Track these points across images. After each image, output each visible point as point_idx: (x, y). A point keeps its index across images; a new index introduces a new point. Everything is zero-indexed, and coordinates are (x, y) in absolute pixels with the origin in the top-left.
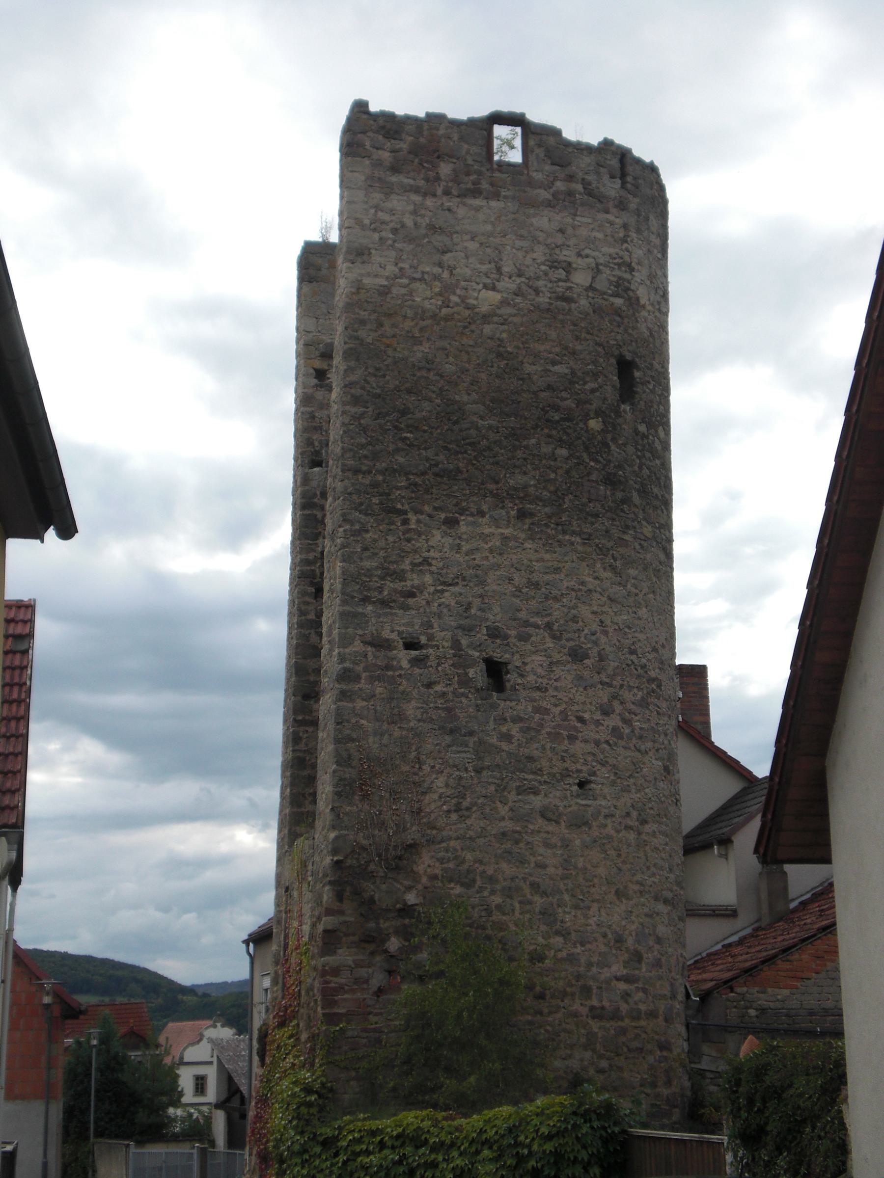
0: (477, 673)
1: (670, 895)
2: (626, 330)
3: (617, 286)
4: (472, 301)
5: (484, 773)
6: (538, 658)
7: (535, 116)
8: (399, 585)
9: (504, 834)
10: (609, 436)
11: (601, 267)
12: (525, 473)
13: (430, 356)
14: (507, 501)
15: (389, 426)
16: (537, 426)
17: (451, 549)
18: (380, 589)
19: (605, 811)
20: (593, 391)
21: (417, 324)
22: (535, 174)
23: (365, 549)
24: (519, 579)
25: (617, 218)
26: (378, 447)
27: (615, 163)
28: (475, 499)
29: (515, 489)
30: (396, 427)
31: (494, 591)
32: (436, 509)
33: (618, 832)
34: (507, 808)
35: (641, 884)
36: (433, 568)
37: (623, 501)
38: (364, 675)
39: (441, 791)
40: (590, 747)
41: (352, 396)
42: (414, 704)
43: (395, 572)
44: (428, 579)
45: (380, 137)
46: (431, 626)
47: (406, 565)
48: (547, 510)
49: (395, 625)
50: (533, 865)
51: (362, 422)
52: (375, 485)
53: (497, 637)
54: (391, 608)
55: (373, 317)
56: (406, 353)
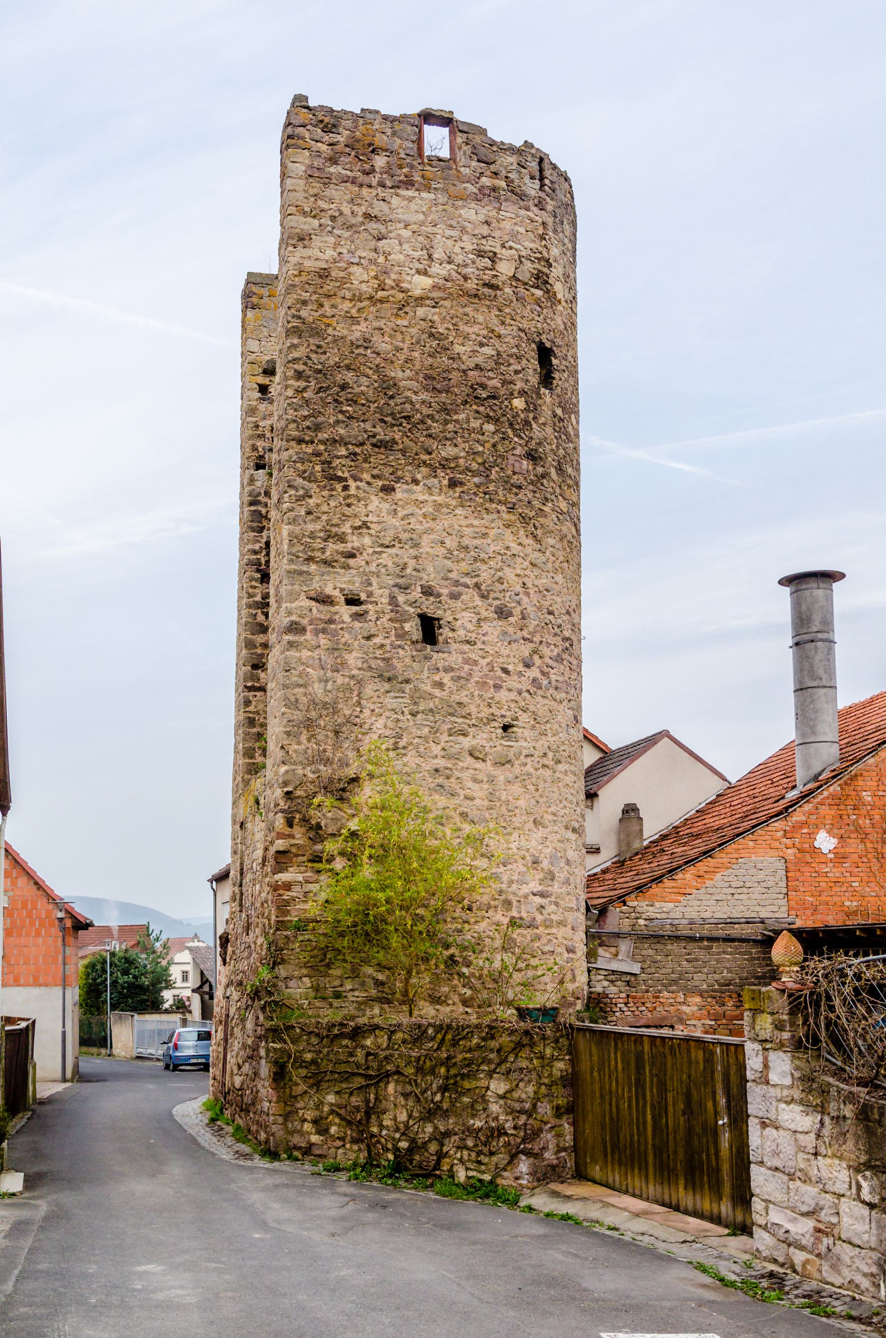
0: (413, 627)
1: (577, 825)
3: (538, 278)
5: (420, 716)
8: (340, 547)
9: (437, 770)
10: (531, 415)
12: (456, 446)
13: (367, 335)
14: (439, 471)
15: (330, 399)
16: (466, 402)
17: (389, 513)
19: (525, 752)
20: (517, 372)
21: (354, 306)
22: (462, 169)
23: (309, 513)
24: (450, 543)
26: (321, 419)
27: (534, 165)
28: (410, 468)
29: (447, 460)
30: (336, 401)
31: (427, 553)
32: (374, 477)
33: (536, 769)
34: (439, 747)
35: (555, 814)
36: (372, 532)
38: (309, 628)
39: (380, 732)
40: (513, 695)
41: (296, 371)
42: (354, 654)
43: (336, 535)
46: (370, 584)
48: (476, 480)
49: (334, 584)
50: (462, 797)
51: (305, 395)
53: (431, 595)
54: (333, 567)
55: (314, 297)
56: (345, 332)
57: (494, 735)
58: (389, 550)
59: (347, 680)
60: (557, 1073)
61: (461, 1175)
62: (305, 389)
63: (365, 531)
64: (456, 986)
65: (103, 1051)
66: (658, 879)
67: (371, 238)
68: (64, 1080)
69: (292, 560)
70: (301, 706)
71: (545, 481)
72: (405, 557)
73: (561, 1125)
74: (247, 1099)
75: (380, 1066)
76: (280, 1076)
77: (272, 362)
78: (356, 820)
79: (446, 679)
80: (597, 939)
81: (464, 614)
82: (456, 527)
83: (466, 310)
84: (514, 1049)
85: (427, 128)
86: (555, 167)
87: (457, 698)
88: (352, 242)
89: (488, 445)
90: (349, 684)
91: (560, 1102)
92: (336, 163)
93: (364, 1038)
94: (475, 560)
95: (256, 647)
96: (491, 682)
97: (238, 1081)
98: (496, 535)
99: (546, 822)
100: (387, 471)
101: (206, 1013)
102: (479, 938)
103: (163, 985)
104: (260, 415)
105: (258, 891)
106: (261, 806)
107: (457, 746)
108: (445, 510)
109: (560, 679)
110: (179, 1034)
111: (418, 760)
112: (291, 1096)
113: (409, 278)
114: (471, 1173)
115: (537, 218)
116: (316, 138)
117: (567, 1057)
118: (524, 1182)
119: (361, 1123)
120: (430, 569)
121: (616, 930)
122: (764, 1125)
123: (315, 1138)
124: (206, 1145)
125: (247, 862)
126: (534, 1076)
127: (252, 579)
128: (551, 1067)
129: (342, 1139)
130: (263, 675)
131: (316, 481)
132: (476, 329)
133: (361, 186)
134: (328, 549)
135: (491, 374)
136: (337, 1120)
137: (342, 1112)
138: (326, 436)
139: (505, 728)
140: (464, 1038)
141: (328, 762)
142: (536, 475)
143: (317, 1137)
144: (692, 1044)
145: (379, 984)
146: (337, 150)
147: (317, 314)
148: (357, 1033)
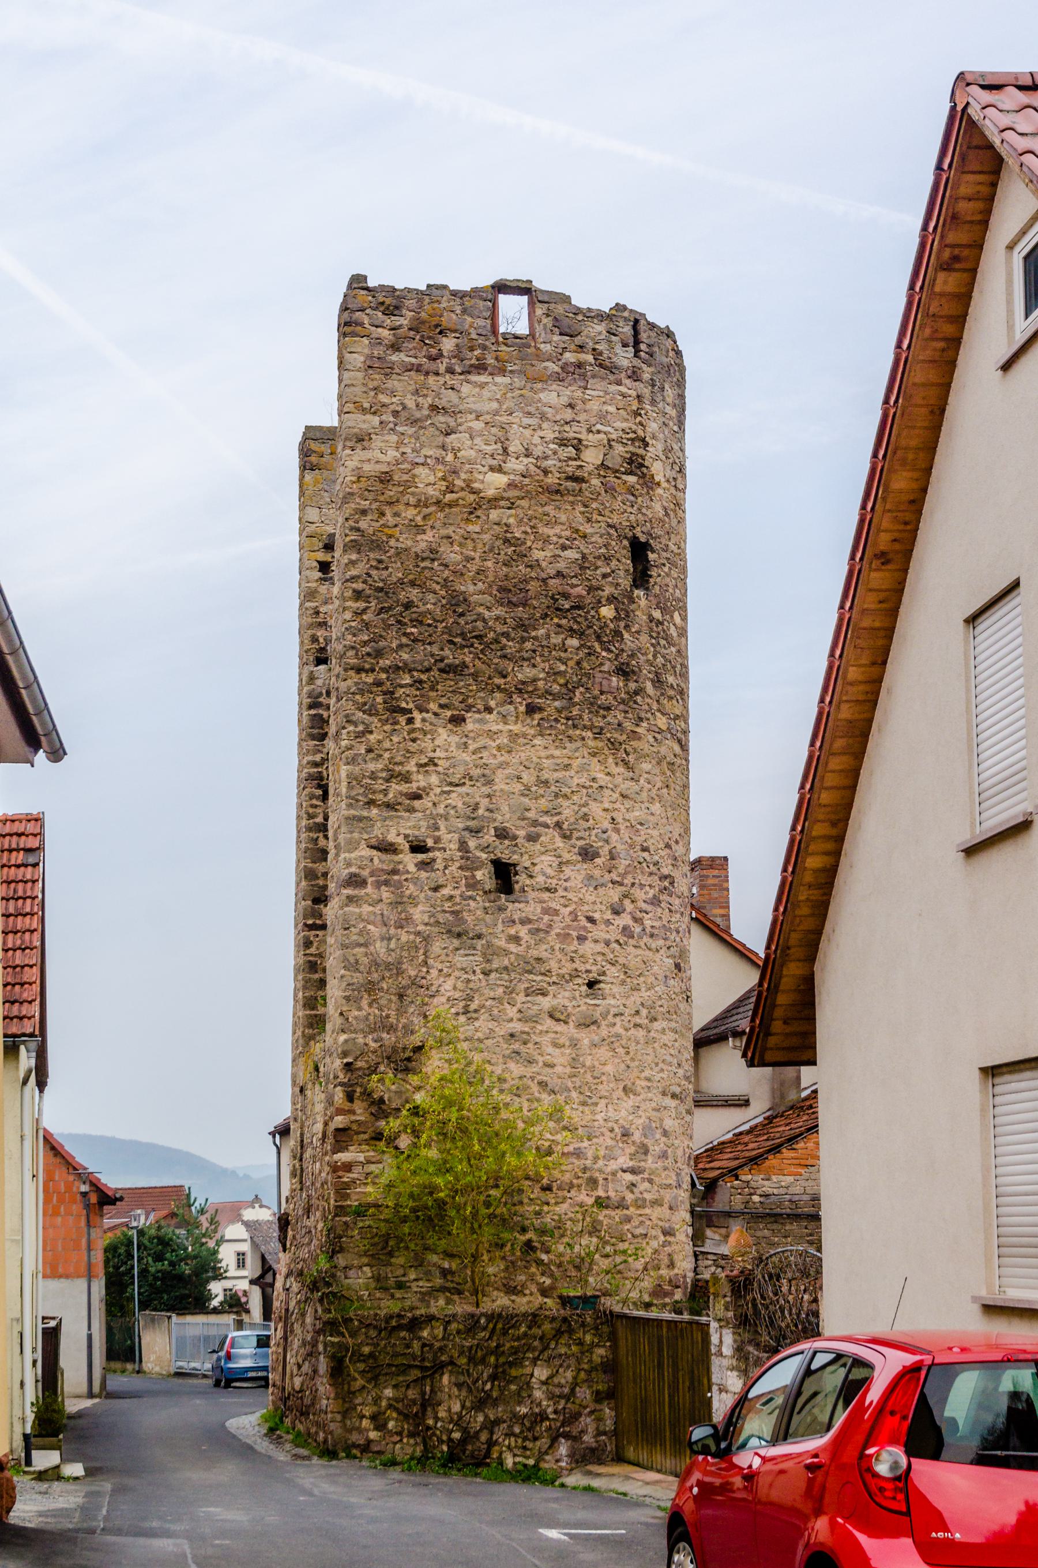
0: (484, 875)
4: (476, 485)
5: (493, 975)
7: (538, 284)
8: (404, 787)
9: (512, 1035)
10: (622, 624)
11: (613, 443)
12: (534, 666)
15: (392, 621)
16: (546, 615)
17: (458, 747)
18: (385, 792)
19: (613, 1011)
20: (605, 576)
21: (419, 513)
22: (542, 346)
24: (528, 777)
25: (629, 387)
26: (382, 644)
27: (627, 330)
28: (482, 694)
29: (524, 683)
30: (399, 622)
31: (502, 790)
32: (441, 706)
34: (515, 1009)
35: (648, 1080)
36: (440, 769)
37: (636, 693)
38: (370, 880)
39: (449, 994)
40: (600, 947)
41: (354, 591)
42: (420, 908)
43: (400, 774)
44: (434, 779)
46: (438, 829)
48: (557, 704)
49: (397, 830)
50: (541, 1064)
51: (364, 617)
52: (378, 683)
53: (505, 838)
54: (396, 810)
55: (374, 506)
56: (409, 543)
57: (577, 994)
58: (458, 789)
59: (412, 937)
60: (597, 1359)
61: (509, 1461)
62: (364, 611)
63: (431, 768)
64: (534, 1274)
65: (129, 1366)
66: (776, 1149)
67: (437, 433)
68: (91, 1395)
69: (351, 804)
70: (362, 968)
71: (639, 699)
72: (477, 796)
73: (601, 1410)
74: (307, 1401)
75: (435, 1357)
76: (337, 1371)
77: (332, 536)
78: (423, 1093)
79: (523, 932)
80: (705, 1218)
81: (543, 858)
82: (535, 759)
83: (546, 509)
84: (554, 1336)
85: (501, 297)
86: (652, 326)
87: (535, 953)
88: (417, 439)
89: (571, 663)
90: (414, 942)
91: (600, 1387)
92: (399, 350)
93: (421, 1329)
94: (556, 796)
95: (318, 878)
96: (574, 934)
97: (297, 1382)
98: (578, 765)
99: (639, 1089)
100: (456, 700)
101: (267, 1314)
102: (560, 1221)
103: (210, 1274)
104: (320, 598)
105: (318, 1169)
106: (321, 1074)
107: (536, 1007)
108: (521, 740)
109: (657, 924)
110: (233, 1338)
111: (491, 1025)
112: (350, 1392)
113: (481, 477)
114: (518, 1459)
115: (630, 392)
116: (376, 323)
117: (608, 1344)
118: (563, 1464)
119: (416, 1416)
120: (505, 808)
121: (727, 1209)
122: (721, 1391)
123: (373, 1435)
124: (263, 1451)
125: (307, 1135)
126: (572, 1361)
127: (312, 797)
128: (591, 1353)
129: (400, 1434)
130: (325, 911)
131: (377, 714)
132: (557, 530)
133: (427, 373)
134: (391, 791)
135: (574, 581)
136: (395, 1415)
137: (400, 1406)
138: (388, 662)
139: (591, 984)
140: (513, 1327)
141: (391, 1029)
142: (628, 693)
143: (375, 1433)
144: (694, 1326)
145: (445, 1273)
146: (399, 333)
147: (378, 524)
148: (415, 1324)
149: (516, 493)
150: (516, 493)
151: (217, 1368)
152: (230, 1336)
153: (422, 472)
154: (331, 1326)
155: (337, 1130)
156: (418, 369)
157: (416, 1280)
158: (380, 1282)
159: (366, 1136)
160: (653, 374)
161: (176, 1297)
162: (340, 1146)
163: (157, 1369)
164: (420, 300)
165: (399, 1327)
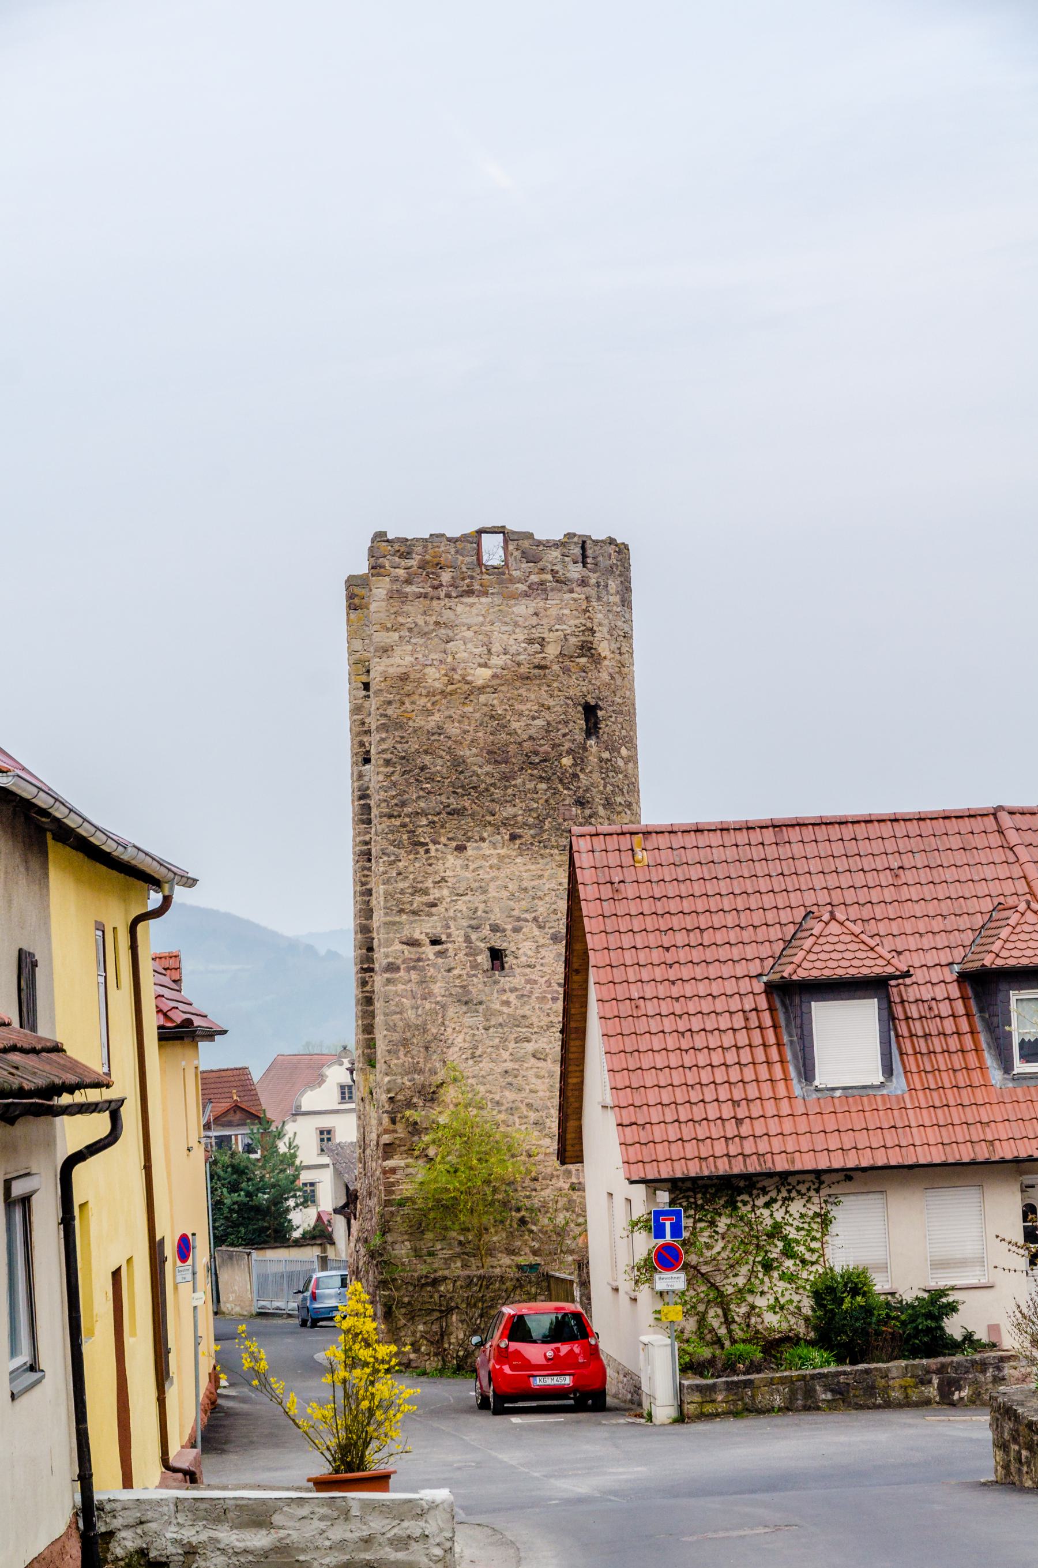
2: (548, 816)
4: (469, 678)
5: (492, 1030)
6: (528, 944)
7: (511, 527)
8: (425, 899)
9: (506, 1072)
10: (578, 768)
13: (440, 724)
15: (412, 780)
16: (522, 768)
17: (462, 867)
18: (411, 903)
20: (564, 735)
23: (399, 874)
24: (512, 886)
25: (579, 594)
26: (406, 796)
27: (577, 551)
28: (477, 829)
29: (507, 819)
30: (417, 780)
32: (449, 839)
34: (508, 1053)
36: (449, 884)
37: (590, 817)
38: (402, 966)
42: (439, 984)
44: (445, 892)
45: (397, 559)
46: (449, 928)
47: (429, 884)
48: (532, 832)
52: (404, 825)
55: (398, 697)
56: (423, 723)
59: (433, 1006)
62: (393, 773)
70: (398, 1029)
75: (448, 1303)
79: (512, 997)
81: (525, 943)
82: (517, 873)
83: (520, 691)
87: (520, 1012)
88: (426, 647)
89: (541, 801)
92: (411, 584)
94: (533, 898)
96: (549, 996)
104: (365, 712)
110: (318, 1279)
113: (472, 672)
123: (412, 1356)
129: (428, 1354)
131: (403, 848)
132: (529, 705)
133: (432, 599)
134: (418, 901)
135: (542, 742)
136: (425, 1342)
137: (428, 1336)
138: (410, 810)
141: (420, 1072)
146: (412, 574)
148: (435, 1282)
149: (498, 681)
150: (498, 681)
151: (303, 1308)
152: (314, 1277)
153: (430, 671)
154: (383, 1284)
155: (386, 1145)
156: (425, 596)
157: (442, 1249)
158: (417, 1253)
159: (406, 1148)
160: (598, 577)
161: (254, 1230)
162: (387, 1156)
163: (238, 1309)
164: (425, 547)
165: (426, 1284)
